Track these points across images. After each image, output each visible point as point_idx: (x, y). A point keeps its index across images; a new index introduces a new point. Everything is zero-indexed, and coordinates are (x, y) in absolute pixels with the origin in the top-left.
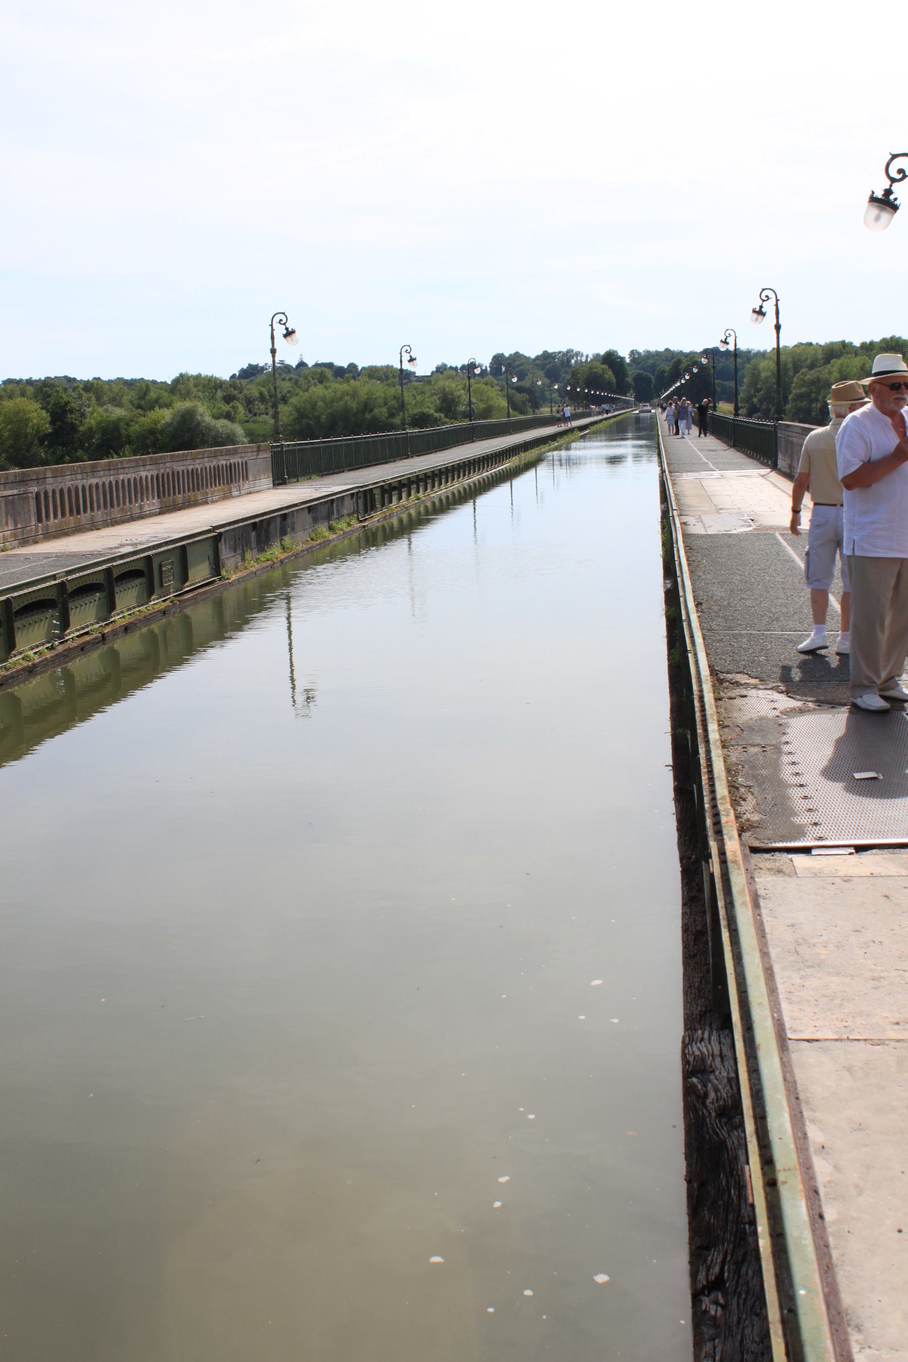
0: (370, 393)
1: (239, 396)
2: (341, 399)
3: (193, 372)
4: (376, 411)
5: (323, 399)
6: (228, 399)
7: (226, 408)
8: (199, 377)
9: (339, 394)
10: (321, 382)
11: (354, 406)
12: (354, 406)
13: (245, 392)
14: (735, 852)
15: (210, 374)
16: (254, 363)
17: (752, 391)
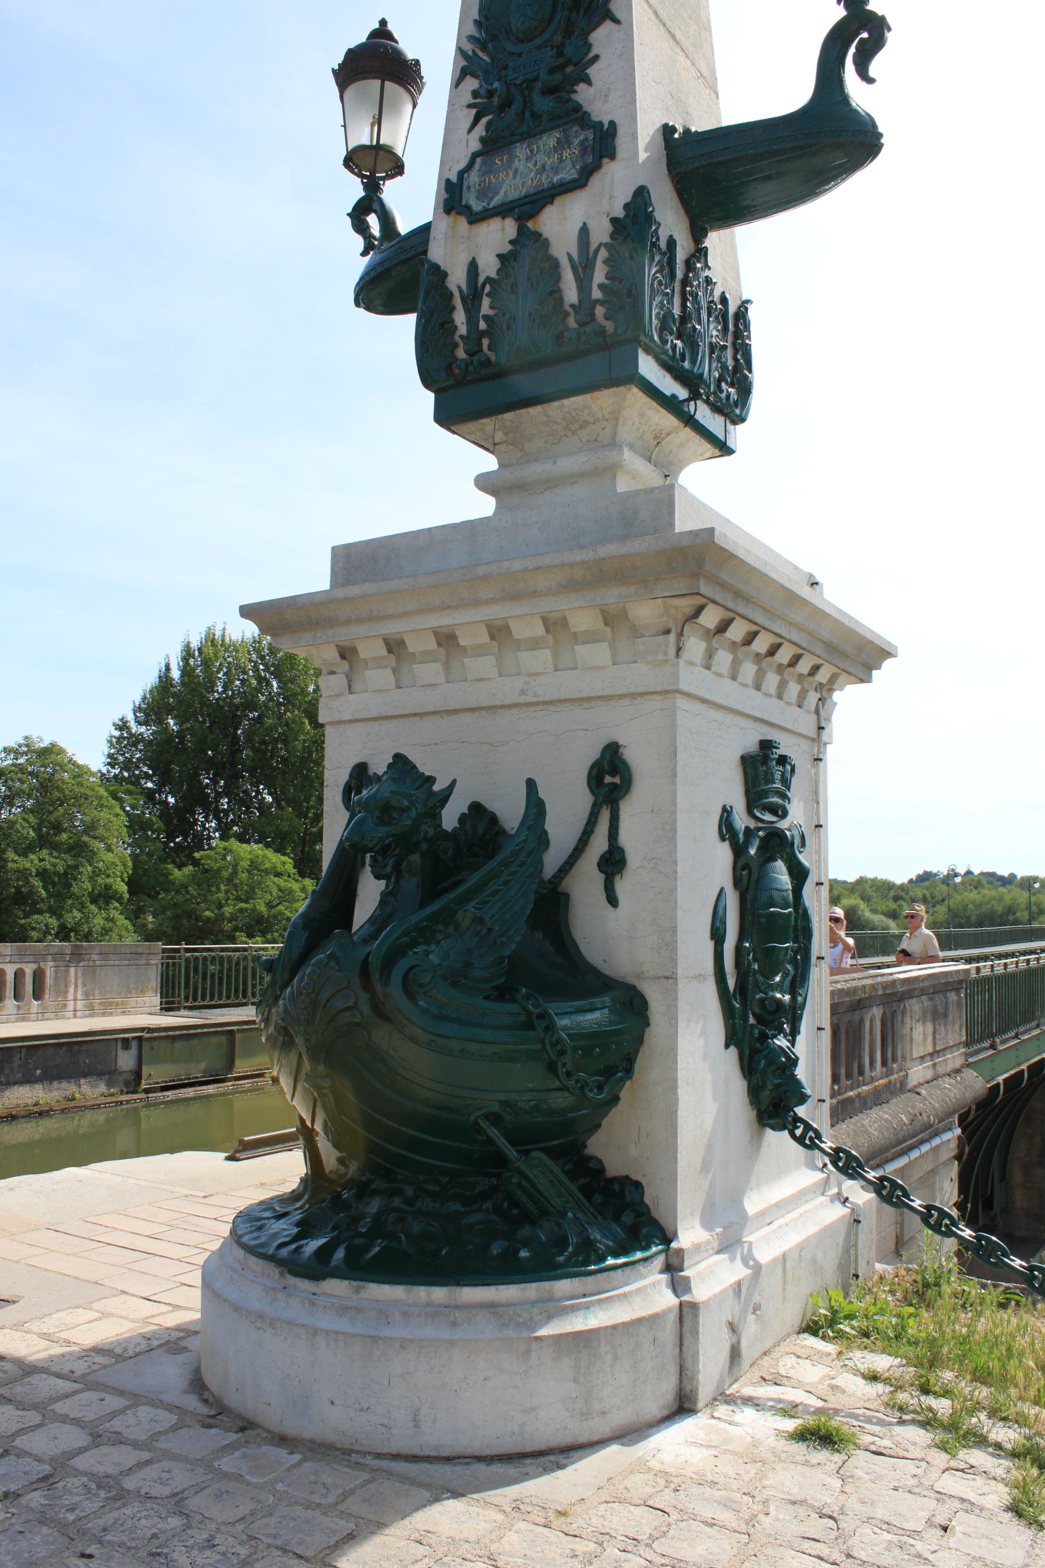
0: (1014, 899)
1: (905, 896)
2: (989, 902)
3: (870, 875)
4: (1018, 914)
5: (974, 902)
6: (896, 899)
7: (893, 905)
8: (874, 880)
9: (987, 899)
10: (976, 888)
11: (1000, 909)
12: (1000, 909)
13: (911, 893)
14: (1012, 1260)
15: (884, 878)
16: (928, 870)
17: (101, 864)
